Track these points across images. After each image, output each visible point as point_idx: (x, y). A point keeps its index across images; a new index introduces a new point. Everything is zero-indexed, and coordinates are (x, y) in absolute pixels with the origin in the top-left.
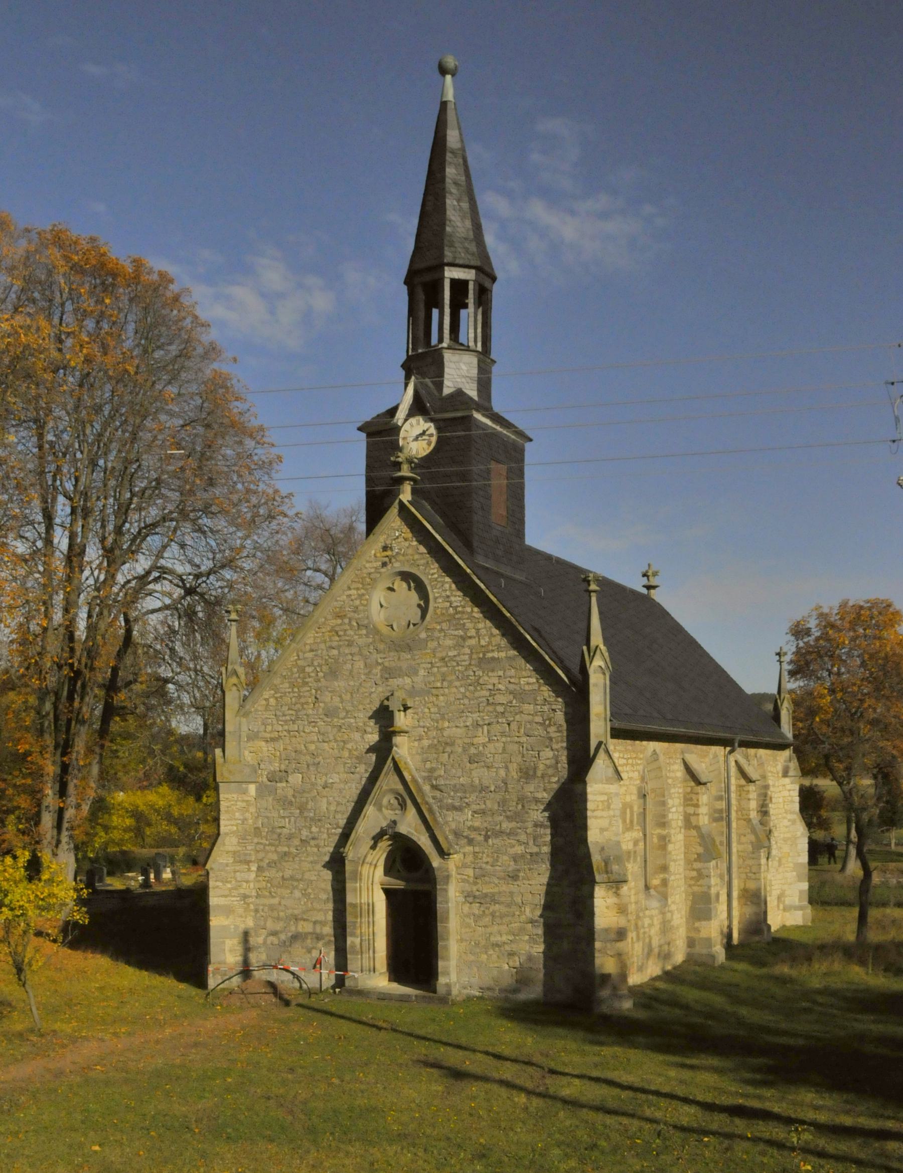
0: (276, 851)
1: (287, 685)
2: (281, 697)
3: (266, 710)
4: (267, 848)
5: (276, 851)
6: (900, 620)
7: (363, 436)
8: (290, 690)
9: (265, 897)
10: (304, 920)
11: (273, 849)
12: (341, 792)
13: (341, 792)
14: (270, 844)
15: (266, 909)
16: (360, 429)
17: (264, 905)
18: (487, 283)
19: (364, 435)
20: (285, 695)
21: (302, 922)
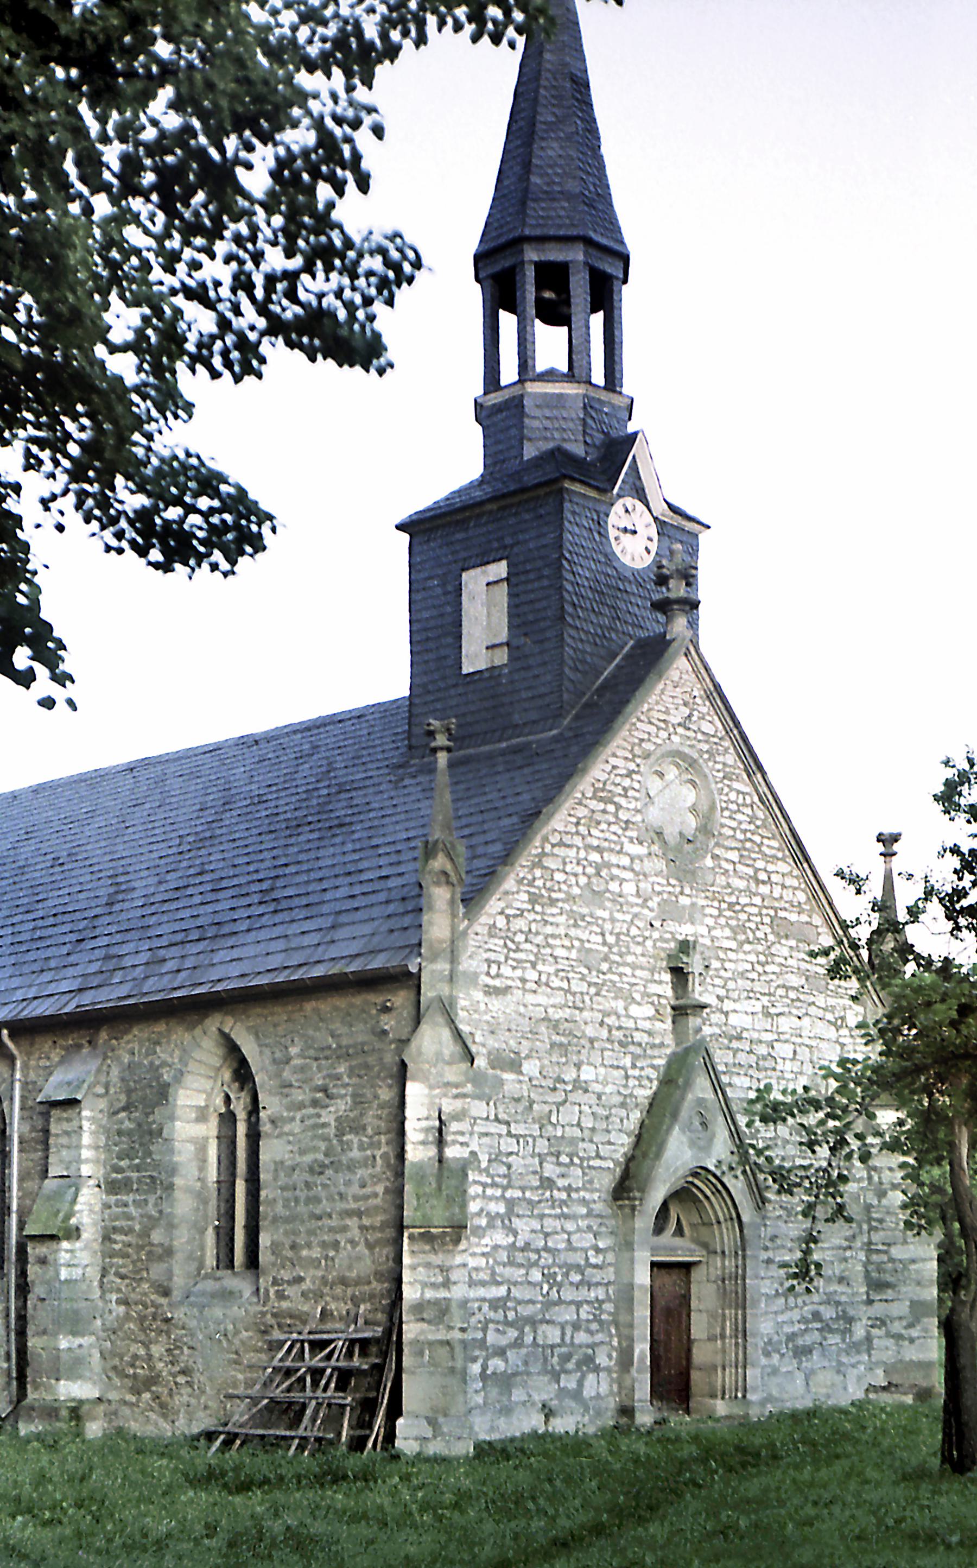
0: (503, 1196)
1: (525, 897)
2: (515, 916)
3: (491, 936)
4: (489, 1192)
5: (503, 1196)
6: (974, 1463)
7: (405, 538)
8: (530, 907)
9: (483, 1284)
10: (548, 1322)
11: (498, 1193)
12: (599, 1098)
13: (599, 1098)
14: (494, 1185)
15: (486, 1307)
16: (400, 527)
17: (484, 1300)
18: (611, 267)
19: (406, 537)
20: (521, 915)
21: (544, 1326)
